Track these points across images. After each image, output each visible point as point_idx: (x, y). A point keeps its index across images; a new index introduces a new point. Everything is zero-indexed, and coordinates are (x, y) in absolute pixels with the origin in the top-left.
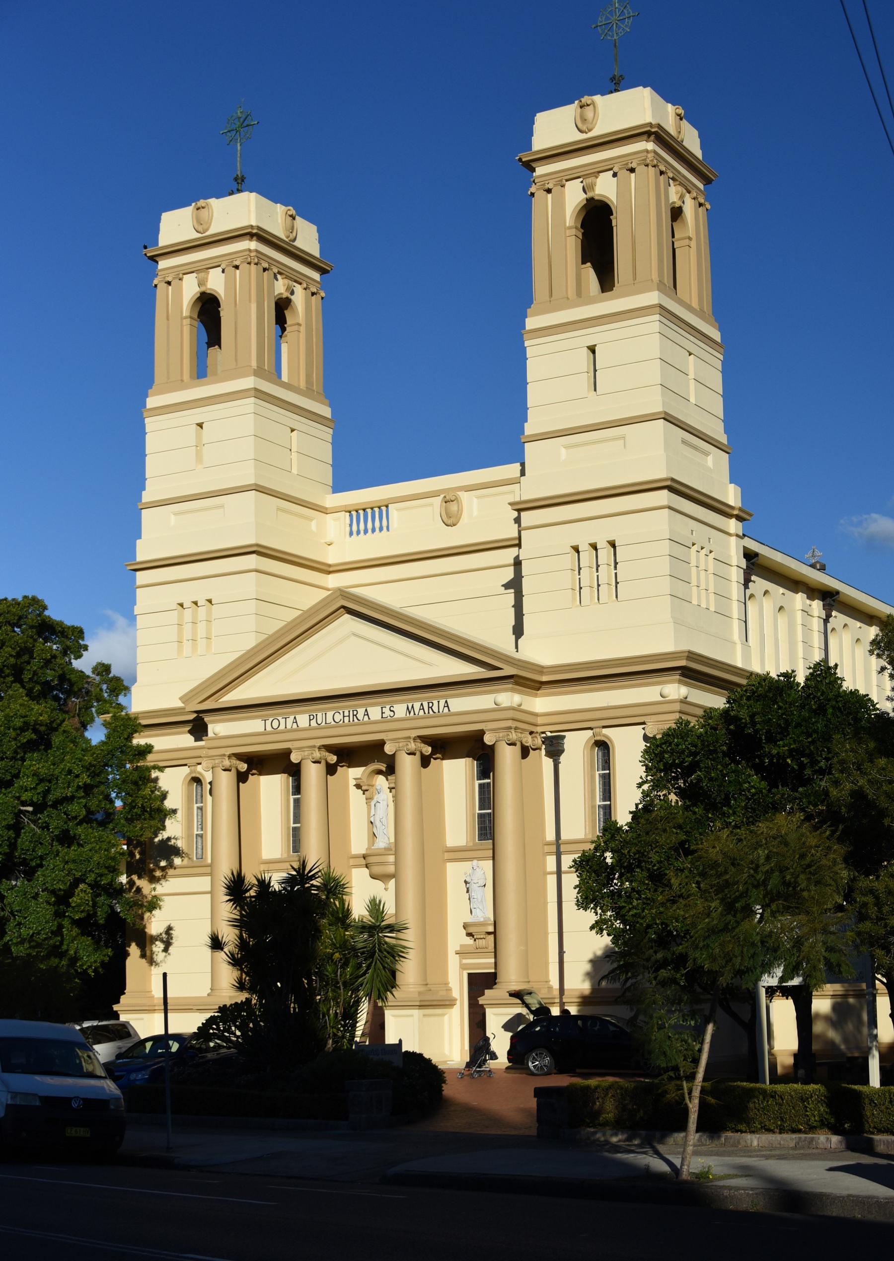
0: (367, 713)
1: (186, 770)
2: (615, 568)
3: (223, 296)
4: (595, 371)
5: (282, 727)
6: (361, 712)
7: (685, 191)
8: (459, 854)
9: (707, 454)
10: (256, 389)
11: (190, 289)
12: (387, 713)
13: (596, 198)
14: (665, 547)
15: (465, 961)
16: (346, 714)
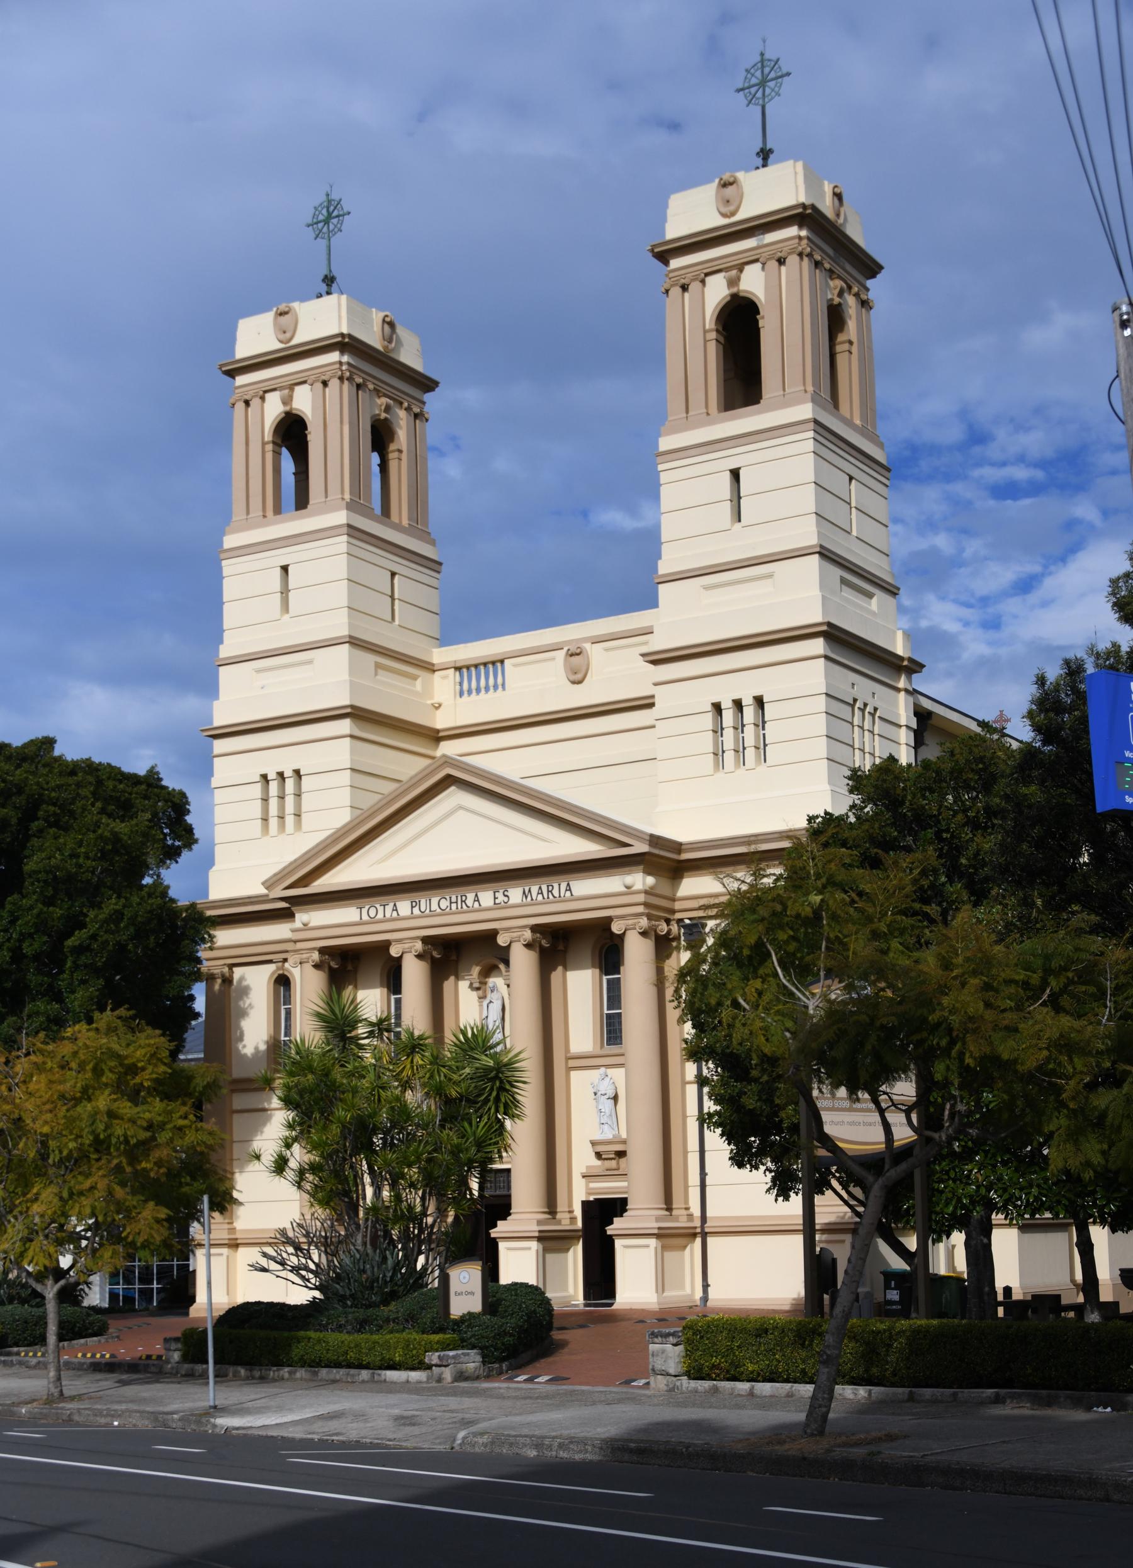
0: (477, 899)
1: (272, 967)
2: (763, 729)
3: (310, 416)
4: (739, 498)
5: (380, 916)
6: (470, 897)
7: (845, 285)
8: (585, 1062)
9: (870, 596)
10: (349, 526)
11: (273, 409)
12: (501, 898)
13: (741, 294)
14: (821, 703)
15: (592, 1185)
16: (454, 899)
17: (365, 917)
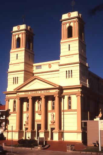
6: (37, 92)
17: (33, 93)
